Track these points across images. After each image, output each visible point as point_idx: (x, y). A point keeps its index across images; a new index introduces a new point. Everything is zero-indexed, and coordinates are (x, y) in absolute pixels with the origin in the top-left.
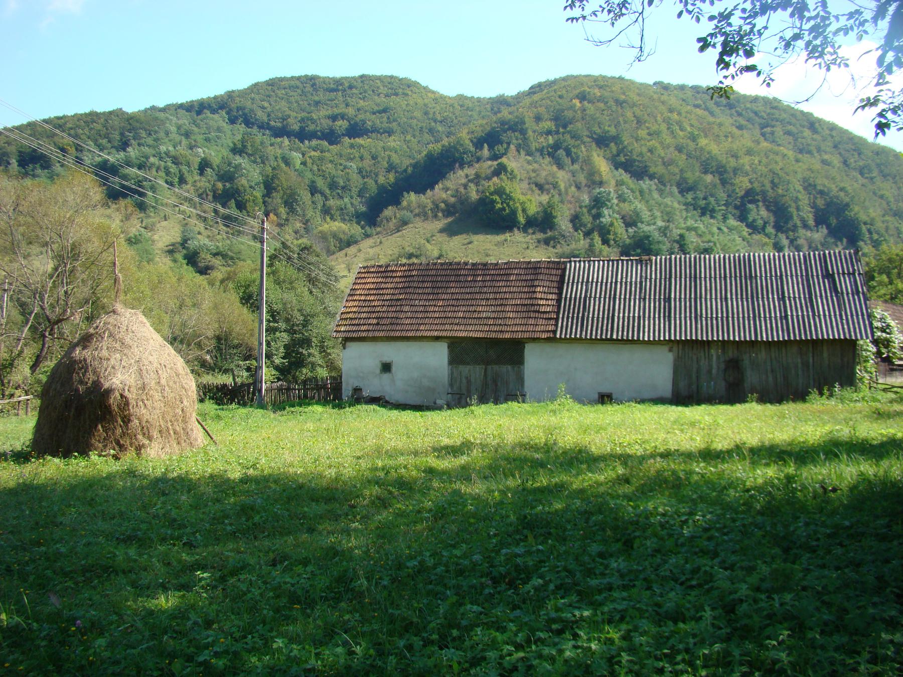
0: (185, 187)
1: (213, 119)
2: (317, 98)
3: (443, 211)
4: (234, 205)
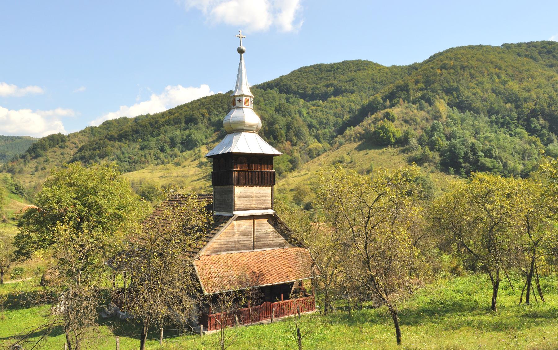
2: (321, 76)
3: (358, 138)
4: (272, 138)
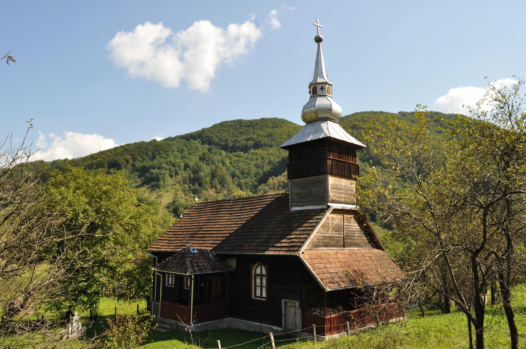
0: (178, 177)
1: (194, 143)
2: (241, 131)
3: (282, 186)
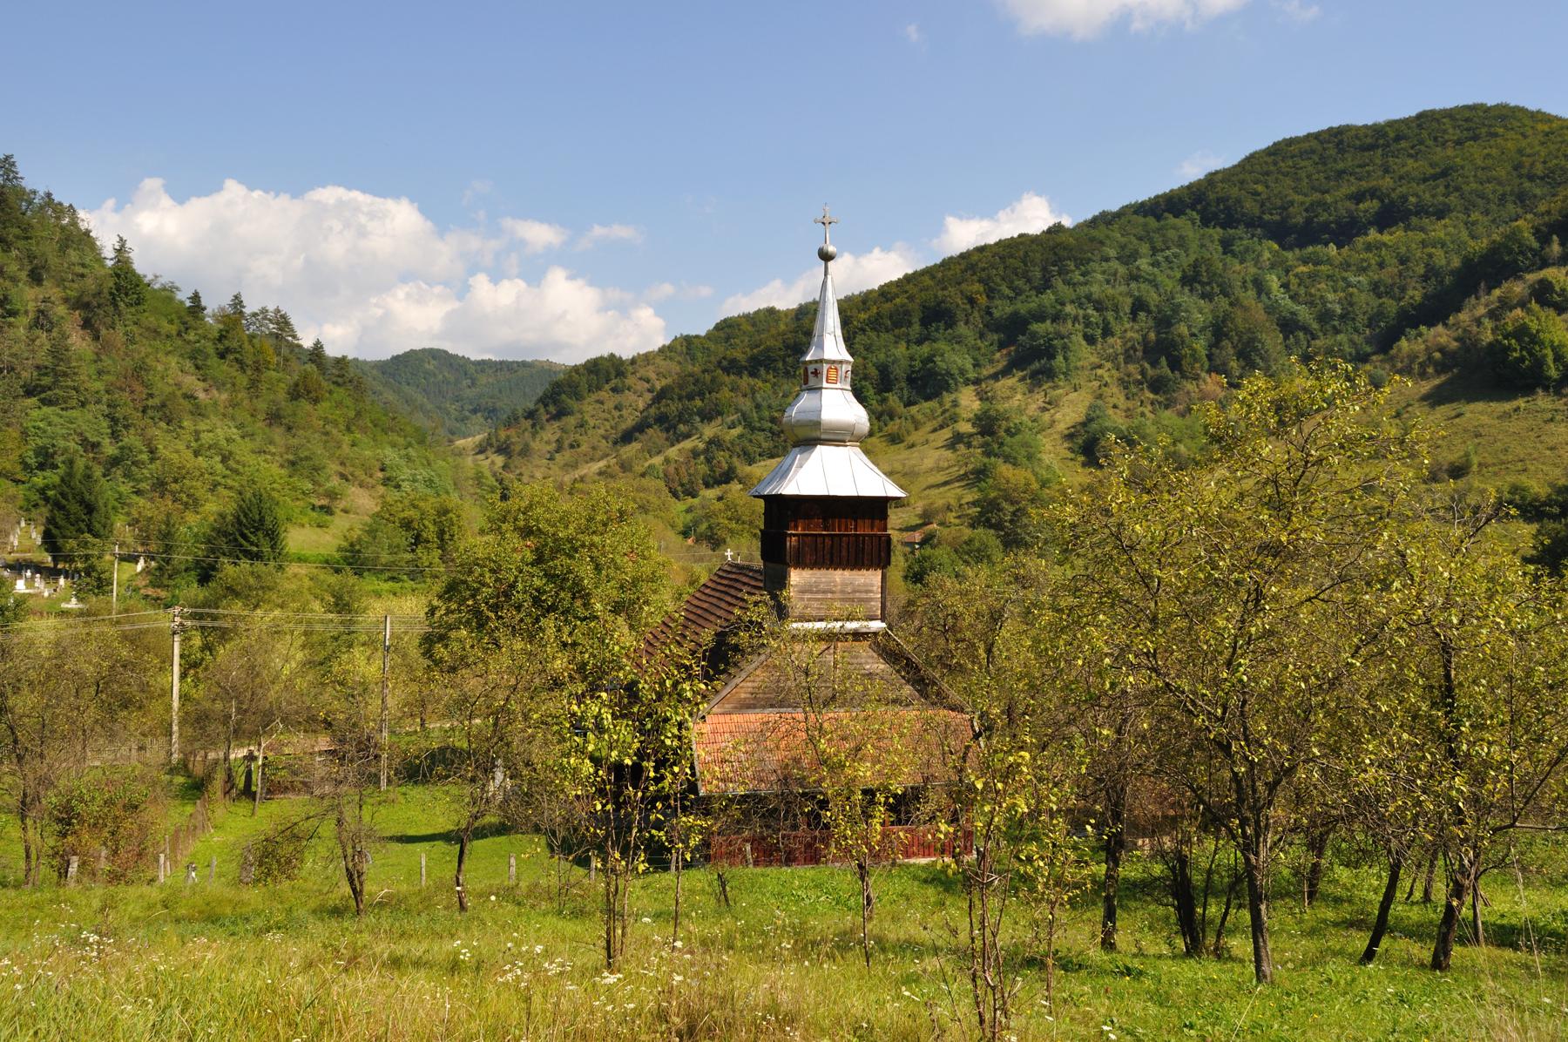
0: (1111, 340)
2: (1341, 166)
